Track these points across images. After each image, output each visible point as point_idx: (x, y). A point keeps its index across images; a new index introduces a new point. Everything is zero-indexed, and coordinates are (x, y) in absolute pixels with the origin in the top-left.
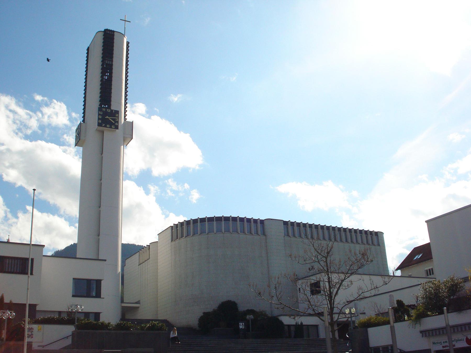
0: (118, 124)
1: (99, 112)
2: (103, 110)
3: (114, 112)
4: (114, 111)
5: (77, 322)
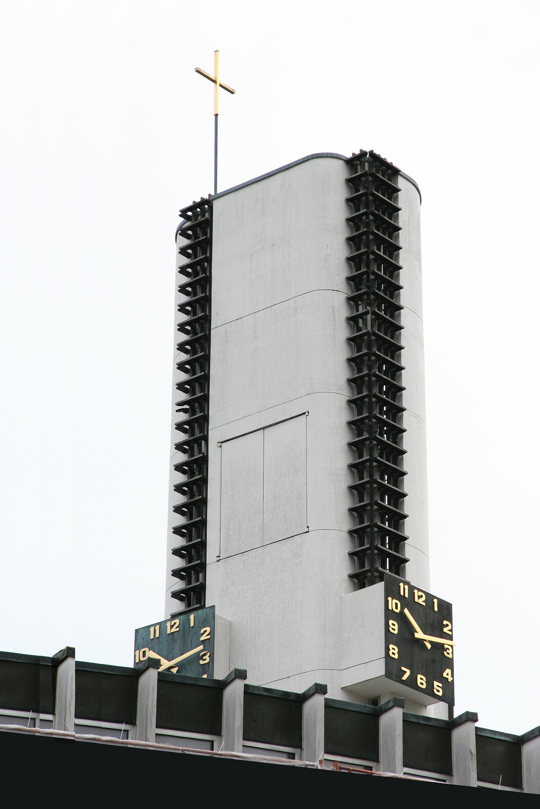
1: (390, 599)
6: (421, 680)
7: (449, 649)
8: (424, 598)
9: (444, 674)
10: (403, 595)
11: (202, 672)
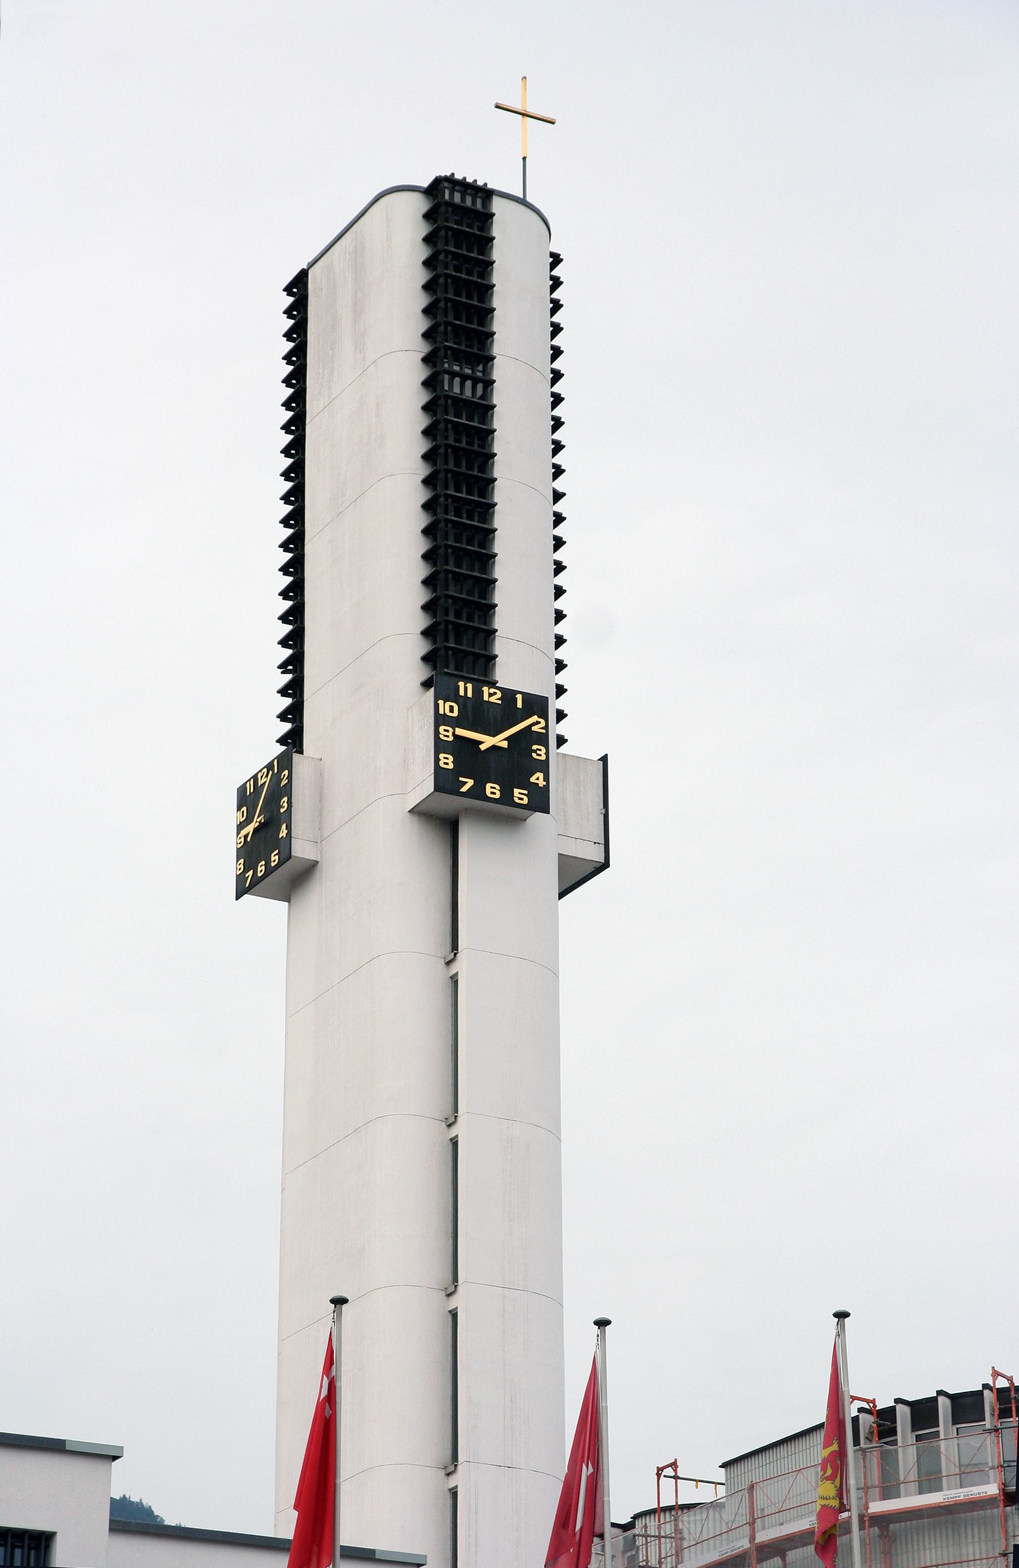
0: (546, 778)
1: (441, 702)
2: (462, 693)
3: (519, 705)
4: (519, 697)
5: (461, 345)
6: (493, 790)
7: (540, 750)
8: (499, 695)
9: (473, 783)
10: (463, 695)
11: (747, 1531)
